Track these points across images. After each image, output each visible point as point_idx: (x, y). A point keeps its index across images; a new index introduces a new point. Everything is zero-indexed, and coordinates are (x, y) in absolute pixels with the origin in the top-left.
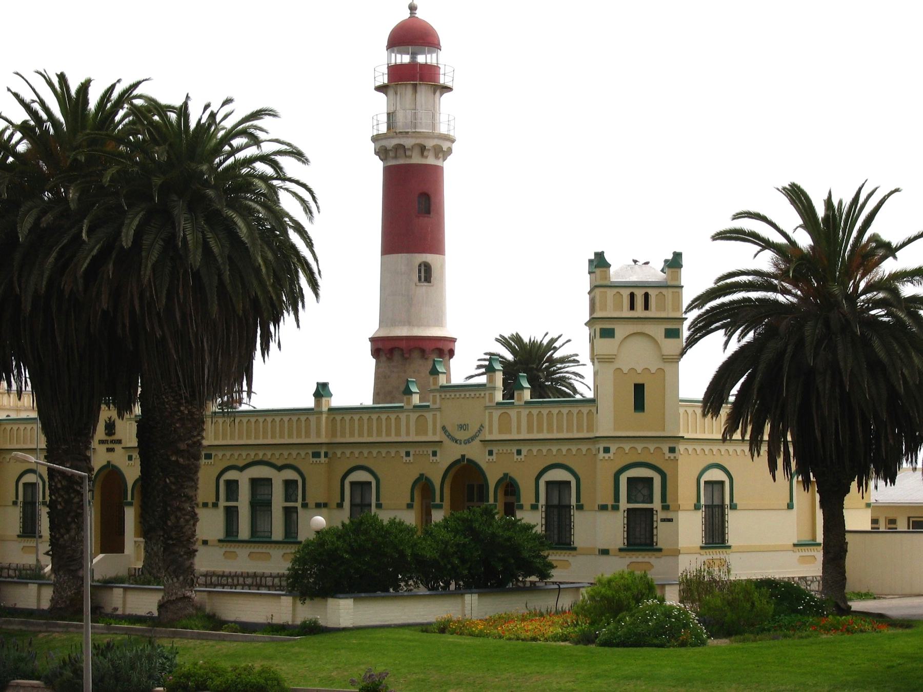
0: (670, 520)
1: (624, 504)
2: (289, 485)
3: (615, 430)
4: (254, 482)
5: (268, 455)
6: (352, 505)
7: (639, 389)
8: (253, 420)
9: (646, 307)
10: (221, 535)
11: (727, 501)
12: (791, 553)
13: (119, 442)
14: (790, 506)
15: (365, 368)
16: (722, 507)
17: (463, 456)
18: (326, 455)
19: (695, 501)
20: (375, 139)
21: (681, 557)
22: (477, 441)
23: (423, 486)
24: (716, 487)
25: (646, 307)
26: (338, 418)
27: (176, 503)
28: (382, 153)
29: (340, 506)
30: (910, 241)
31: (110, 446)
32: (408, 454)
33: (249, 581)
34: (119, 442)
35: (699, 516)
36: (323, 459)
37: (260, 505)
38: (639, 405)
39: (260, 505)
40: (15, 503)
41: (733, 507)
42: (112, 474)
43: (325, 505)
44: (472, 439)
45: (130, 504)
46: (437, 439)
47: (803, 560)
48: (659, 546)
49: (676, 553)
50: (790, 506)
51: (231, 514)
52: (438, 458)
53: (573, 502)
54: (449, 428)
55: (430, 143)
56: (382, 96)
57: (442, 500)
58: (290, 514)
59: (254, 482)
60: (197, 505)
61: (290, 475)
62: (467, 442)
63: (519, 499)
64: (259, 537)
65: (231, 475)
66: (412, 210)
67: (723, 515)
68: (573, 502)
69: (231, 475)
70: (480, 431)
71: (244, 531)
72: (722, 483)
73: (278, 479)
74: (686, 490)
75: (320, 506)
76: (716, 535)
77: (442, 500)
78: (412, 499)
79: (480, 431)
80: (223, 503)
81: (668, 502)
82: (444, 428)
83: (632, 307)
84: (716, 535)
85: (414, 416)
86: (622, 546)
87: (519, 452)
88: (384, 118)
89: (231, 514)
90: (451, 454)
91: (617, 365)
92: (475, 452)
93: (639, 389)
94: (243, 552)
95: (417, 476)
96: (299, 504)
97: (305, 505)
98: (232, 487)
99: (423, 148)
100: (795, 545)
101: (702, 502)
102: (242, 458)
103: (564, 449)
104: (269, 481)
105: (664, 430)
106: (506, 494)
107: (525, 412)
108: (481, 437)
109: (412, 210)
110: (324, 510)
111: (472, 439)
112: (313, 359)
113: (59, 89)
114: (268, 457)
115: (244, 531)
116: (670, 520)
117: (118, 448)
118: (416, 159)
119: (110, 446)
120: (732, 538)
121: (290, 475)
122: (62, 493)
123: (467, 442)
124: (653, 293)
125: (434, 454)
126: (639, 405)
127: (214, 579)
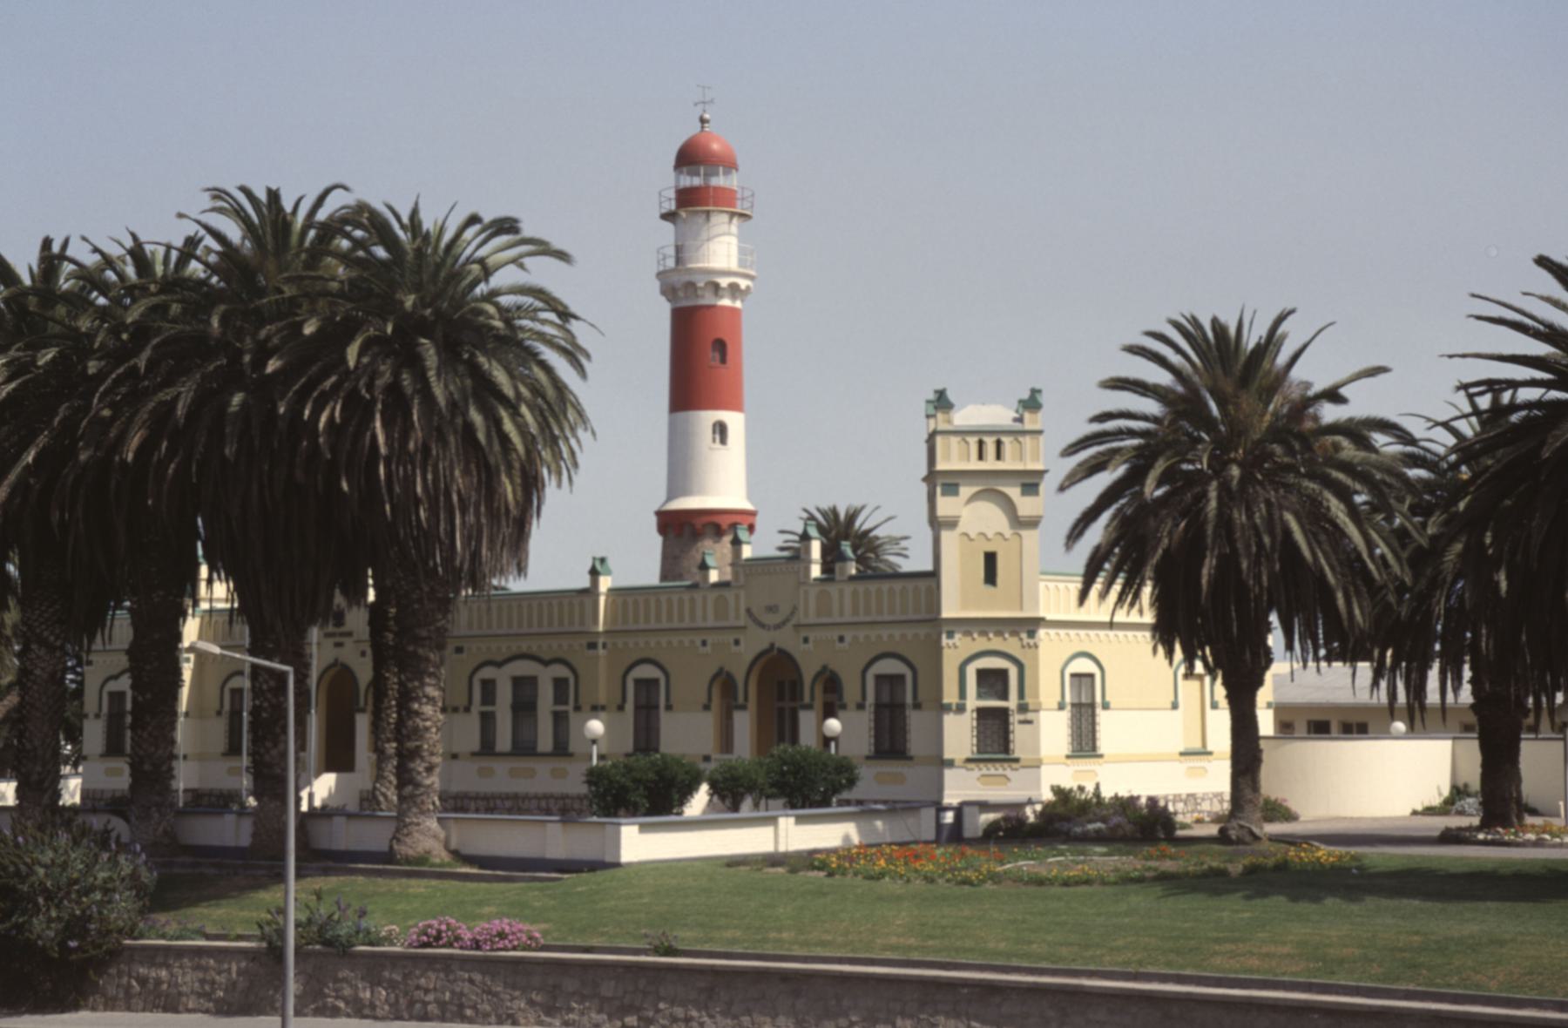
0: (1029, 722)
1: (972, 702)
2: (560, 685)
3: (964, 607)
4: (518, 682)
5: (533, 646)
6: (637, 708)
7: (990, 559)
8: (630, 600)
9: (999, 456)
10: (475, 745)
11: (1098, 699)
12: (1177, 764)
13: (349, 634)
14: (1175, 706)
15: (653, 544)
16: (1092, 706)
17: (772, 645)
18: (604, 646)
19: (1059, 698)
20: (660, 275)
21: (1043, 768)
22: (789, 625)
23: (724, 684)
24: (1084, 680)
25: (999, 456)
26: (630, 600)
27: (416, 706)
28: (669, 291)
29: (621, 708)
30: (1464, 356)
31: (338, 639)
32: (704, 643)
33: (508, 804)
34: (349, 634)
35: (1065, 717)
36: (601, 651)
37: (524, 706)
38: (991, 577)
39: (524, 706)
40: (219, 713)
41: (1106, 706)
42: (340, 677)
43: (603, 708)
44: (784, 623)
45: (363, 711)
46: (741, 623)
47: (110, 772)
48: (1016, 755)
49: (1037, 764)
50: (1175, 706)
51: (487, 720)
52: (742, 647)
53: (909, 699)
54: (754, 610)
55: (724, 282)
56: (668, 227)
57: (746, 699)
58: (560, 719)
59: (518, 682)
60: (86, 716)
61: (561, 671)
62: (778, 627)
63: (841, 697)
64: (524, 748)
65: (488, 673)
66: (699, 360)
67: (1093, 715)
68: (909, 699)
69: (488, 673)
70: (792, 613)
71: (504, 741)
72: (1091, 676)
73: (545, 678)
74: (1049, 686)
75: (596, 710)
76: (1085, 743)
77: (746, 699)
78: (710, 699)
79: (792, 613)
80: (477, 707)
81: (1028, 700)
82: (748, 611)
83: (981, 457)
84: (1085, 743)
85: (712, 596)
86: (969, 755)
87: (841, 639)
88: (671, 251)
89: (487, 720)
90: (754, 642)
91: (961, 528)
92: (786, 639)
93: (990, 559)
94: (501, 767)
95: (714, 670)
96: (570, 708)
97: (577, 708)
98: (489, 687)
99: (716, 287)
100: (1182, 754)
101: (1068, 699)
102: (505, 648)
103: (664, 640)
104: (533, 681)
105: (1021, 608)
106: (826, 691)
107: (848, 589)
108: (794, 621)
109: (699, 360)
110: (603, 714)
111: (784, 623)
112: (586, 535)
113: (172, 266)
114: (534, 650)
115: (504, 741)
116: (1029, 722)
117: (348, 641)
118: (708, 299)
119: (338, 639)
120: (1104, 744)
121: (561, 671)
122: (269, 696)
123: (778, 627)
124: (1006, 440)
125: (737, 642)
126: (991, 577)
127: (543, 804)
